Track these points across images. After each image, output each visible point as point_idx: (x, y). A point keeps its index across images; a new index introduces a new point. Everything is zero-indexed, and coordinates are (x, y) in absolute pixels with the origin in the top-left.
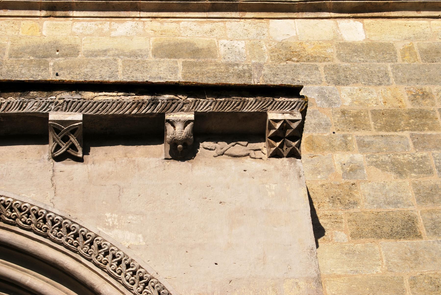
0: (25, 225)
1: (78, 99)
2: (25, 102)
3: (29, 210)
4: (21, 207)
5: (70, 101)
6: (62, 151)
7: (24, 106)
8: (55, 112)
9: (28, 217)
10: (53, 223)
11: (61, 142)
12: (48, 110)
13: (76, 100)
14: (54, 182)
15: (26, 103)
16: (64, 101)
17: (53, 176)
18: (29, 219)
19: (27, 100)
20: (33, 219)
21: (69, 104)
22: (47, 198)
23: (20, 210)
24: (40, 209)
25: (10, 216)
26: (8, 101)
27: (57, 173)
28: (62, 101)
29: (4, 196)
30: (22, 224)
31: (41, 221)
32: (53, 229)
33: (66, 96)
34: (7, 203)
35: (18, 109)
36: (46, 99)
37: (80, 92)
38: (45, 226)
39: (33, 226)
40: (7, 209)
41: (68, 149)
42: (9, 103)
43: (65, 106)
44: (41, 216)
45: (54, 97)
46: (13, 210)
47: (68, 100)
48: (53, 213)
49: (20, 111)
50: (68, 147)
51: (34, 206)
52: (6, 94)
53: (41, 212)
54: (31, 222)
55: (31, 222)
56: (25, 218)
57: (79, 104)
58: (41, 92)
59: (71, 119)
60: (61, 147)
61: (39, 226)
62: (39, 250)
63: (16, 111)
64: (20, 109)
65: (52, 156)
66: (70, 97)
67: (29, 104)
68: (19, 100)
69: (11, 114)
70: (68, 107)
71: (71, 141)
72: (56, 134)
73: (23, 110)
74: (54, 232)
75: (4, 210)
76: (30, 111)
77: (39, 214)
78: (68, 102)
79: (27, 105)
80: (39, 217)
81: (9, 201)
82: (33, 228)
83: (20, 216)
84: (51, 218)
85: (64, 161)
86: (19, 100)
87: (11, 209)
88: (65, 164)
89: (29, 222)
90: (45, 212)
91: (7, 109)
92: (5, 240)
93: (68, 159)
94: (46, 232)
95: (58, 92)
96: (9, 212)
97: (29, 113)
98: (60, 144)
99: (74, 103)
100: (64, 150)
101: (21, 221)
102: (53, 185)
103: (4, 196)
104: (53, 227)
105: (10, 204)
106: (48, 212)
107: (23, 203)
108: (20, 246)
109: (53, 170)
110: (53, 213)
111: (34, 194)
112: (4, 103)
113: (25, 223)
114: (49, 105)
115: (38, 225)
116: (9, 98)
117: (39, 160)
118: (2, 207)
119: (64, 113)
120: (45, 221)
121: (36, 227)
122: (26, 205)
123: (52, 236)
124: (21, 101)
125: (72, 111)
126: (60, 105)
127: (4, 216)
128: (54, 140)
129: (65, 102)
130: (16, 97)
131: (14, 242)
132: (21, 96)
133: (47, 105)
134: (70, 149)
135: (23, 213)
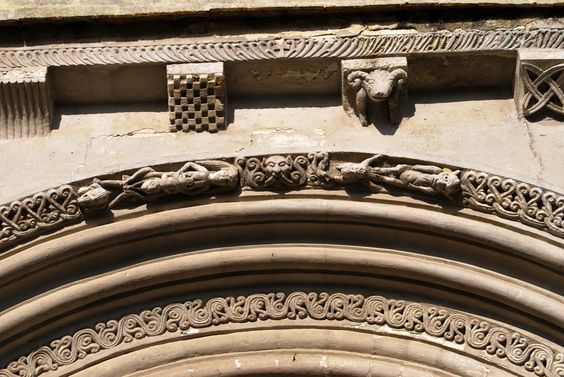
0: (508, 212)
1: (559, 29)
2: (481, 36)
3: (515, 190)
4: (501, 184)
5: (547, 32)
6: (540, 106)
7: (480, 40)
8: (527, 49)
9: (513, 200)
10: (554, 206)
11: (537, 93)
12: (516, 46)
13: (556, 30)
14: (536, 150)
15: (482, 37)
16: (539, 32)
17: (532, 142)
18: (515, 202)
19: (484, 32)
20: (522, 202)
21: (547, 36)
22: (531, 173)
23: (500, 189)
24: (532, 186)
25: (484, 199)
26: (457, 34)
27: (537, 138)
28: (535, 33)
29: (473, 170)
30: (504, 210)
31: (535, 204)
32: (555, 216)
33: (541, 24)
34: (478, 180)
35: (471, 45)
36: (512, 31)
37: (560, 19)
38: (541, 212)
39: (520, 212)
40: (480, 189)
41: (548, 103)
42: (457, 37)
43: (540, 40)
44: (534, 197)
45: (522, 27)
46: (489, 190)
47: (545, 30)
48: (552, 191)
49: (475, 49)
50: (548, 99)
51: (522, 182)
52: (451, 25)
53: (535, 191)
54: (519, 207)
55: (519, 207)
56: (509, 201)
57: (561, 36)
58: (502, 21)
59: (552, 58)
60: (537, 101)
61: (531, 213)
62: (536, 248)
63: (469, 49)
64: (474, 46)
65: (524, 114)
66: (546, 26)
67: (487, 38)
68: (472, 33)
69: (462, 53)
70: (545, 41)
71: (552, 91)
72: (530, 80)
73: (478, 47)
74: (555, 221)
75: (474, 190)
76: (489, 48)
77: (531, 194)
78: (544, 34)
79: (483, 39)
80: (531, 198)
81: (482, 177)
82: (521, 216)
83: (500, 198)
84: (551, 200)
85: (542, 121)
86: (472, 33)
87: (486, 188)
88: (545, 125)
89: (515, 207)
90: (540, 191)
91: (455, 45)
92: (479, 235)
93: (547, 118)
94: (543, 220)
95: (527, 20)
96: (482, 193)
97: (488, 51)
98: (537, 96)
99: (554, 36)
100: (543, 104)
101: (502, 206)
102: (535, 155)
103: (473, 170)
104: (554, 213)
105: (484, 182)
106: (544, 190)
107: (504, 178)
108: (505, 243)
109: (529, 134)
110: (552, 191)
111: (511, 167)
112: (450, 37)
113: (508, 208)
114: (516, 39)
115: (531, 211)
116: (457, 30)
117: (506, 121)
118: (472, 187)
119: (539, 49)
120: (540, 204)
121: (527, 214)
122: (510, 181)
123: (554, 226)
124: (475, 35)
125: (551, 47)
126: (533, 38)
127: (474, 200)
128: (527, 90)
129: (540, 34)
130: (466, 28)
131: (496, 237)
132: (473, 26)
133: (514, 39)
134: (551, 103)
135: (505, 194)
